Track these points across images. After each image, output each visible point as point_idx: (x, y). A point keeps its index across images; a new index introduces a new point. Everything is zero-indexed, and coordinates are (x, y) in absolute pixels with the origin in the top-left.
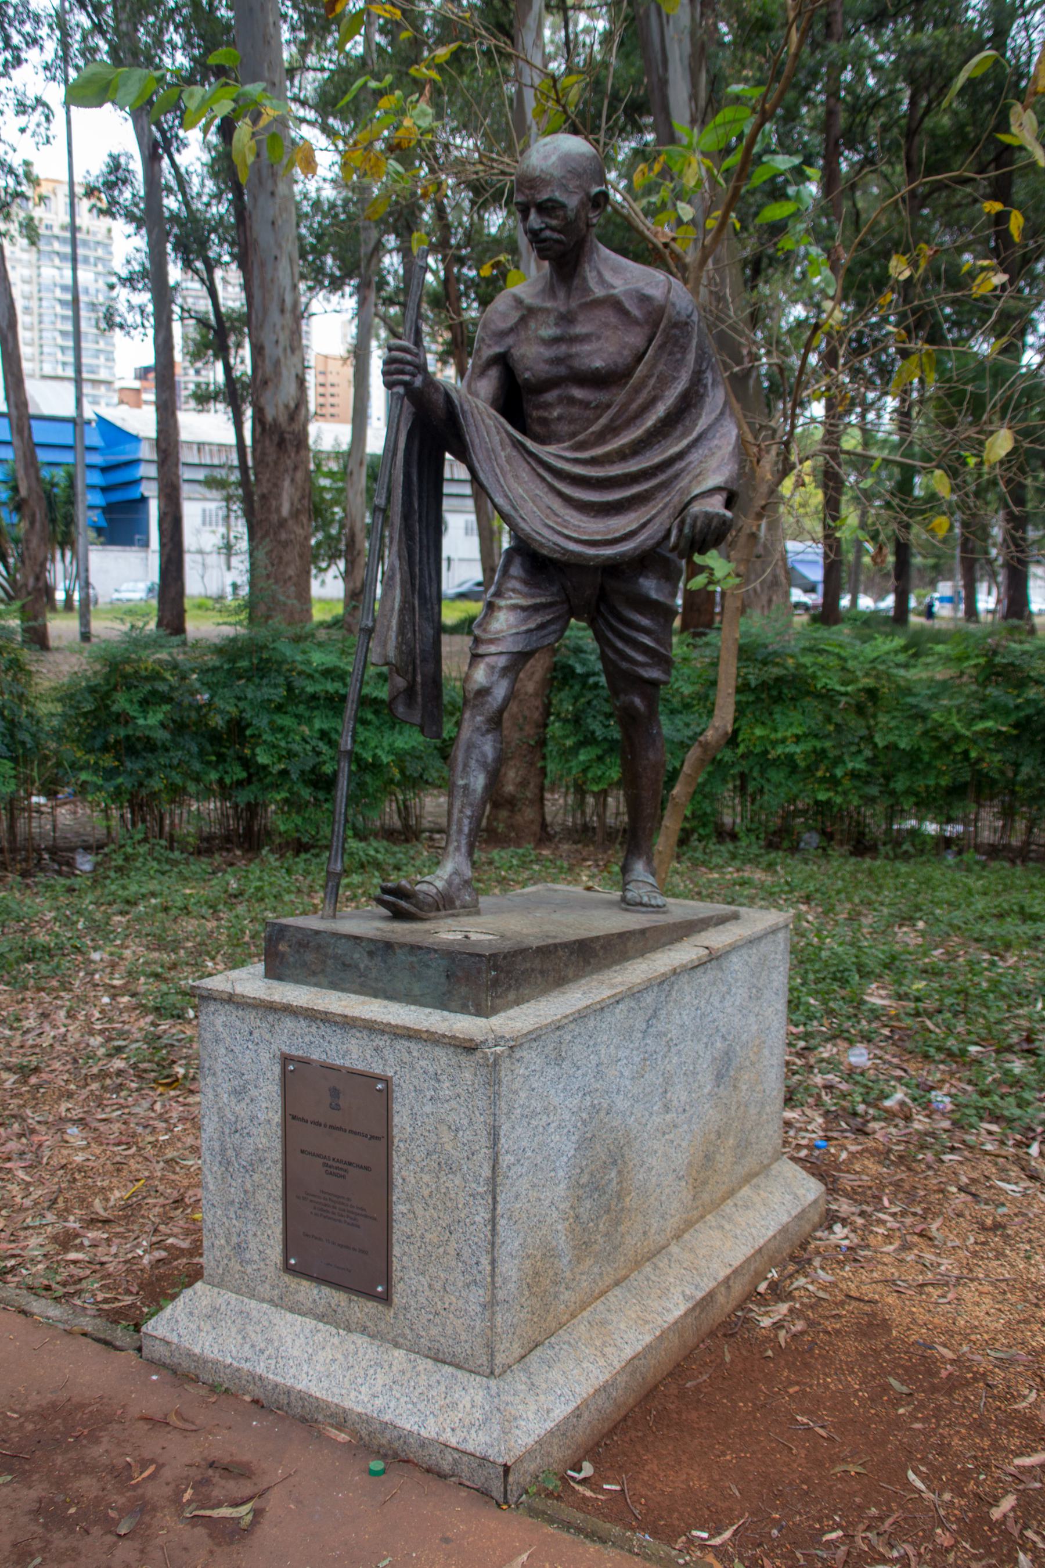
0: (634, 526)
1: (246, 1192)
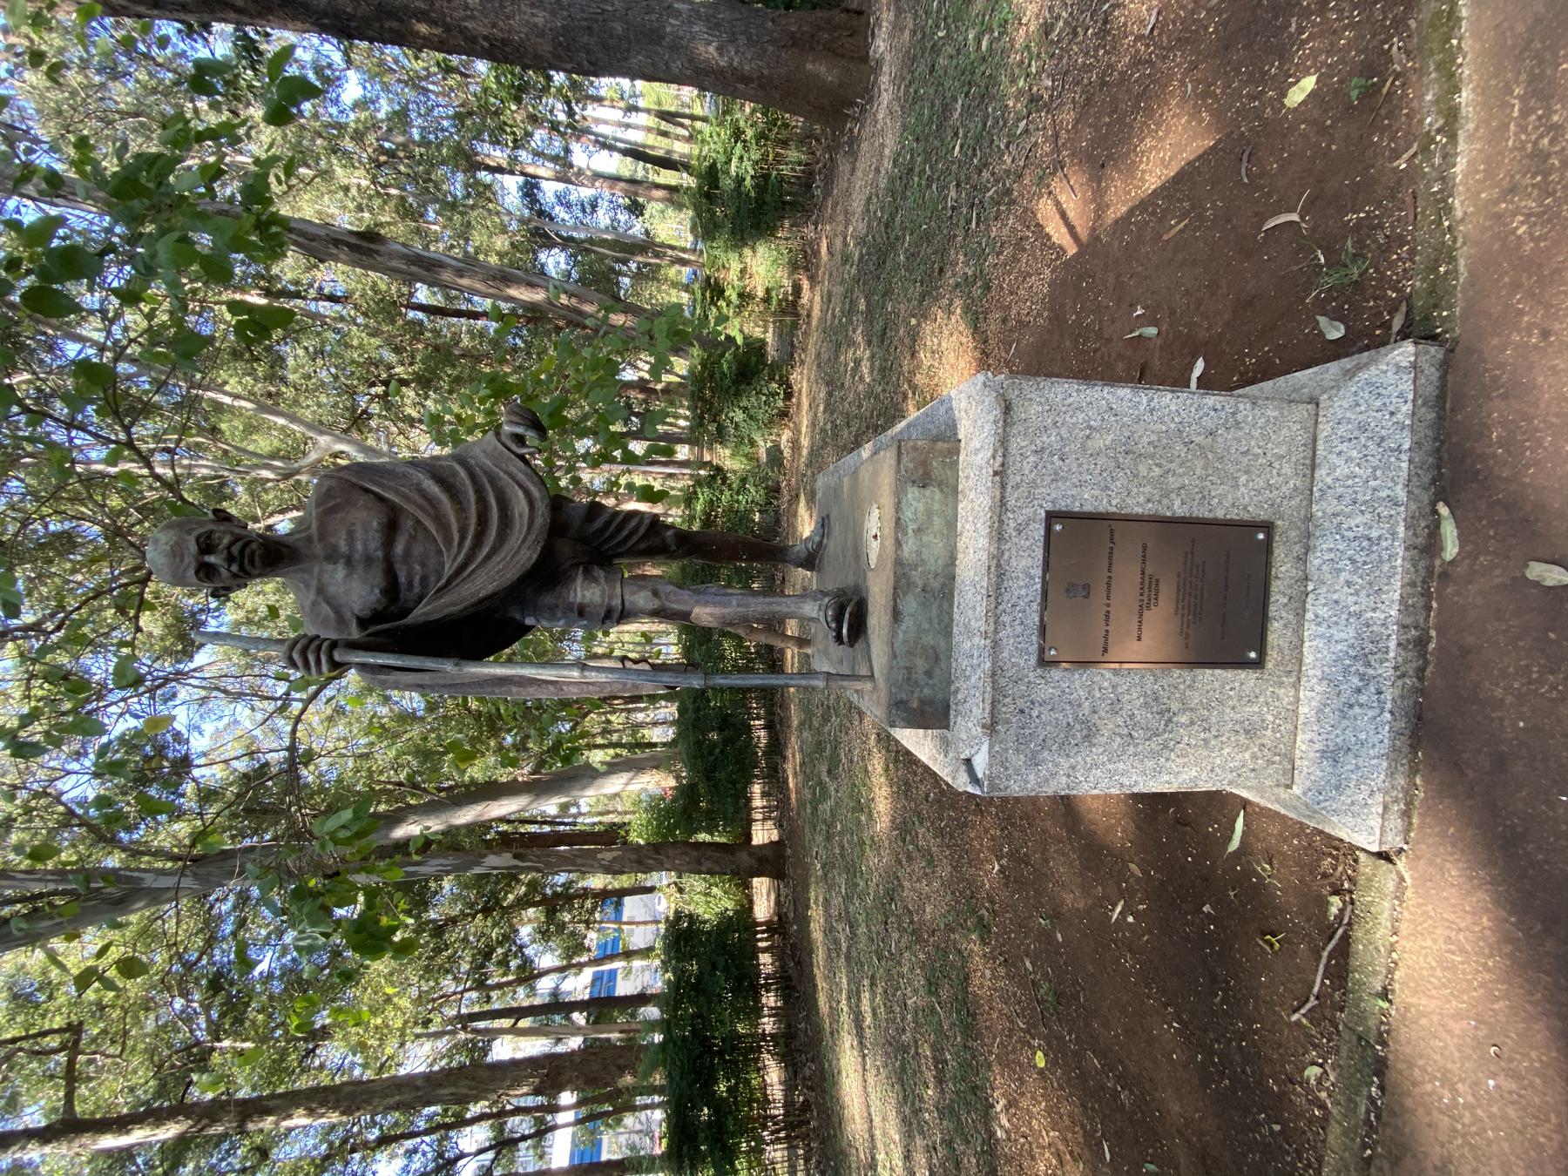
0: (520, 494)
1: (1192, 723)
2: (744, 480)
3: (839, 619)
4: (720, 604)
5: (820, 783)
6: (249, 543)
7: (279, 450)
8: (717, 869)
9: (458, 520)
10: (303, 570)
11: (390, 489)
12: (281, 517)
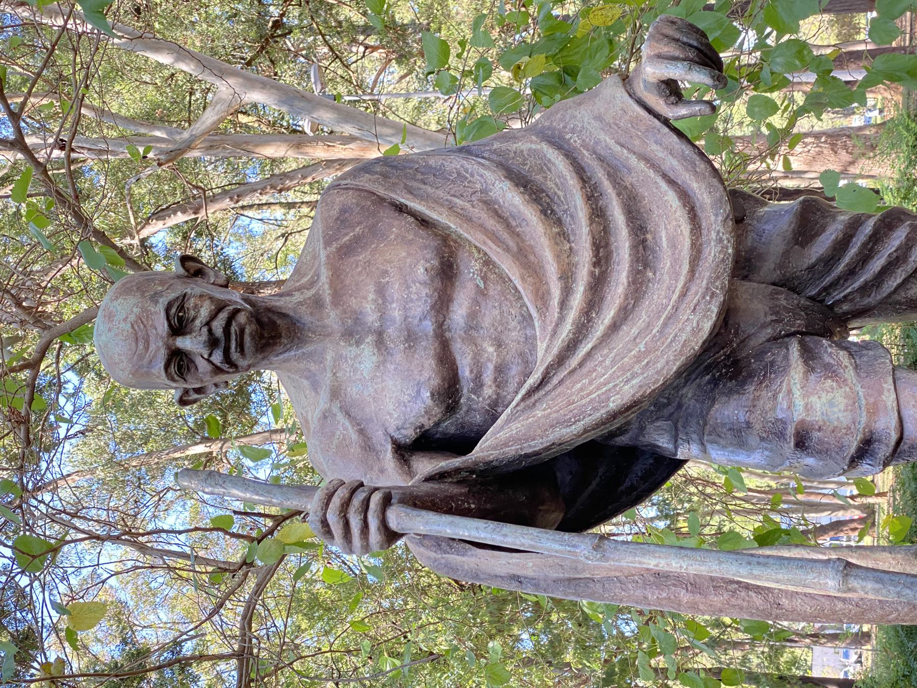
0: (672, 198)
6: (237, 311)
9: (558, 257)
10: (309, 356)
11: (423, 198)
12: (160, 224)
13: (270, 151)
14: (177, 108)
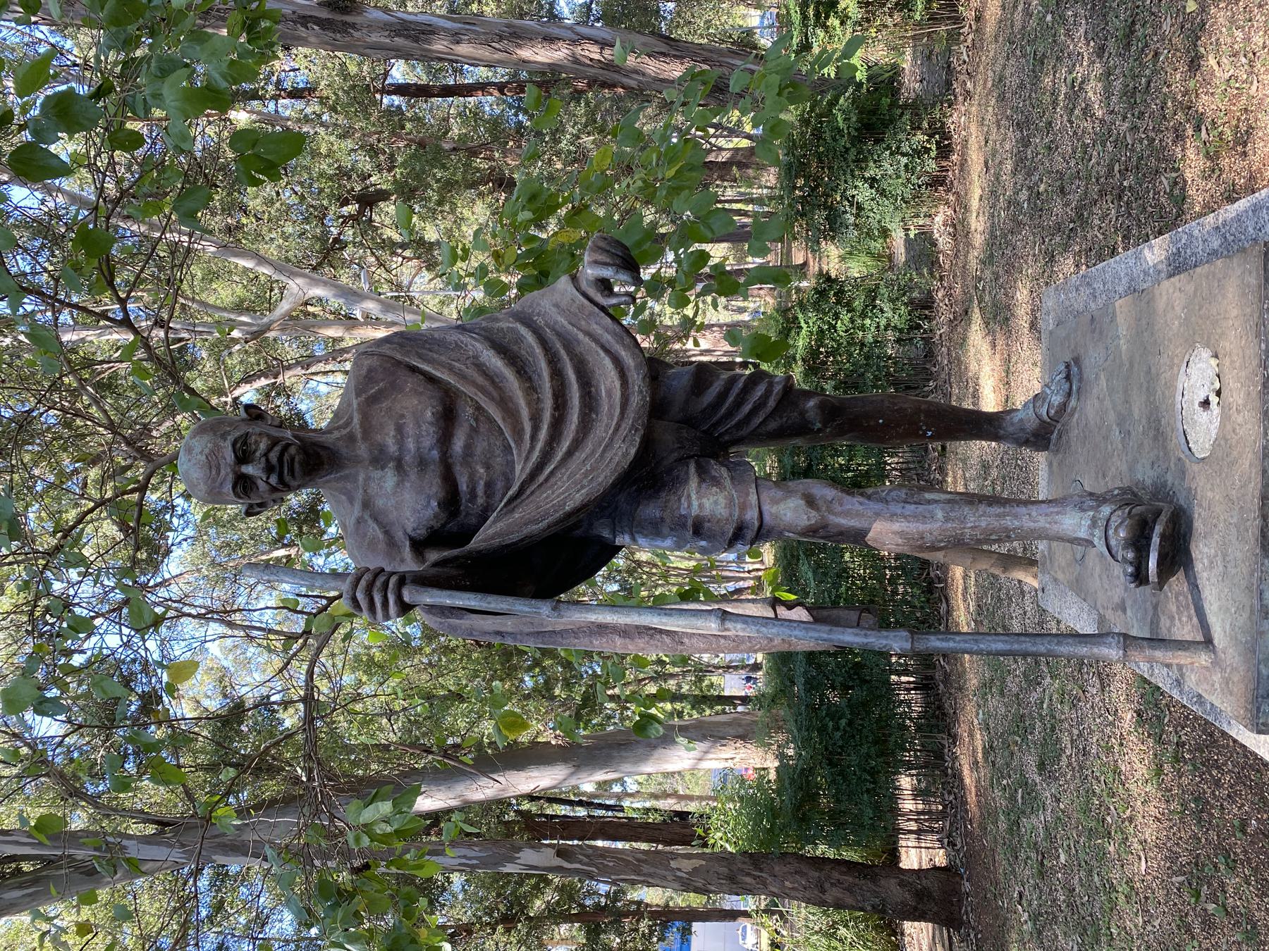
0: (608, 362)
2: (872, 294)
3: (1139, 542)
4: (916, 517)
5: (1024, 783)
6: (287, 446)
7: (242, 301)
8: (850, 900)
9: (529, 404)
10: (346, 478)
11: (441, 365)
13: (332, 332)
14: (259, 300)
